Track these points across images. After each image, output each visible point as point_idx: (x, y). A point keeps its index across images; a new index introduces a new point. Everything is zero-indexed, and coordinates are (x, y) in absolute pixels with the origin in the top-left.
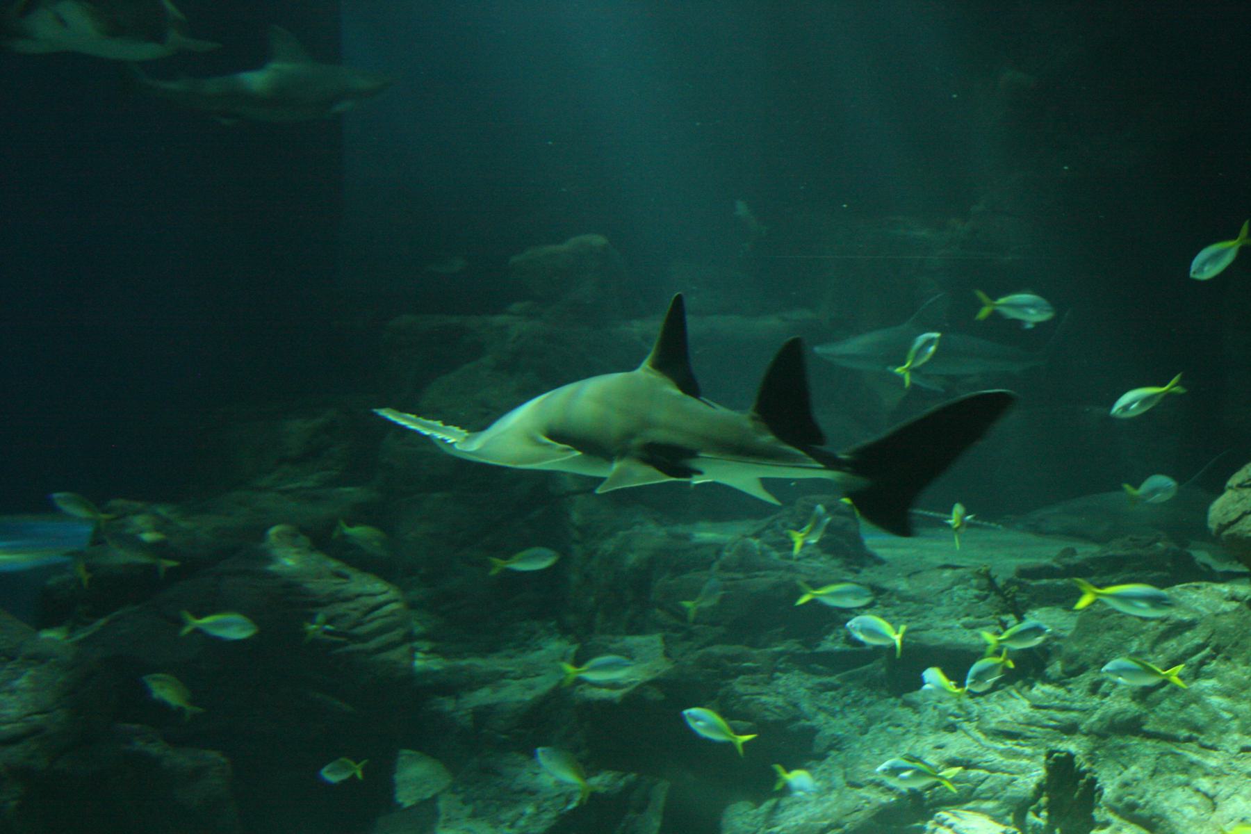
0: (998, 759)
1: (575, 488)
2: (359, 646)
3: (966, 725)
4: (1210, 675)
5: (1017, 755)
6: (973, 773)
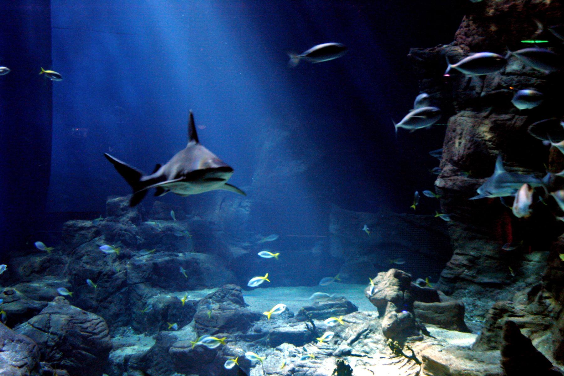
0: (311, 365)
1: (140, 285)
2: (96, 337)
3: (299, 355)
4: (369, 338)
5: (316, 363)
6: (305, 369)
